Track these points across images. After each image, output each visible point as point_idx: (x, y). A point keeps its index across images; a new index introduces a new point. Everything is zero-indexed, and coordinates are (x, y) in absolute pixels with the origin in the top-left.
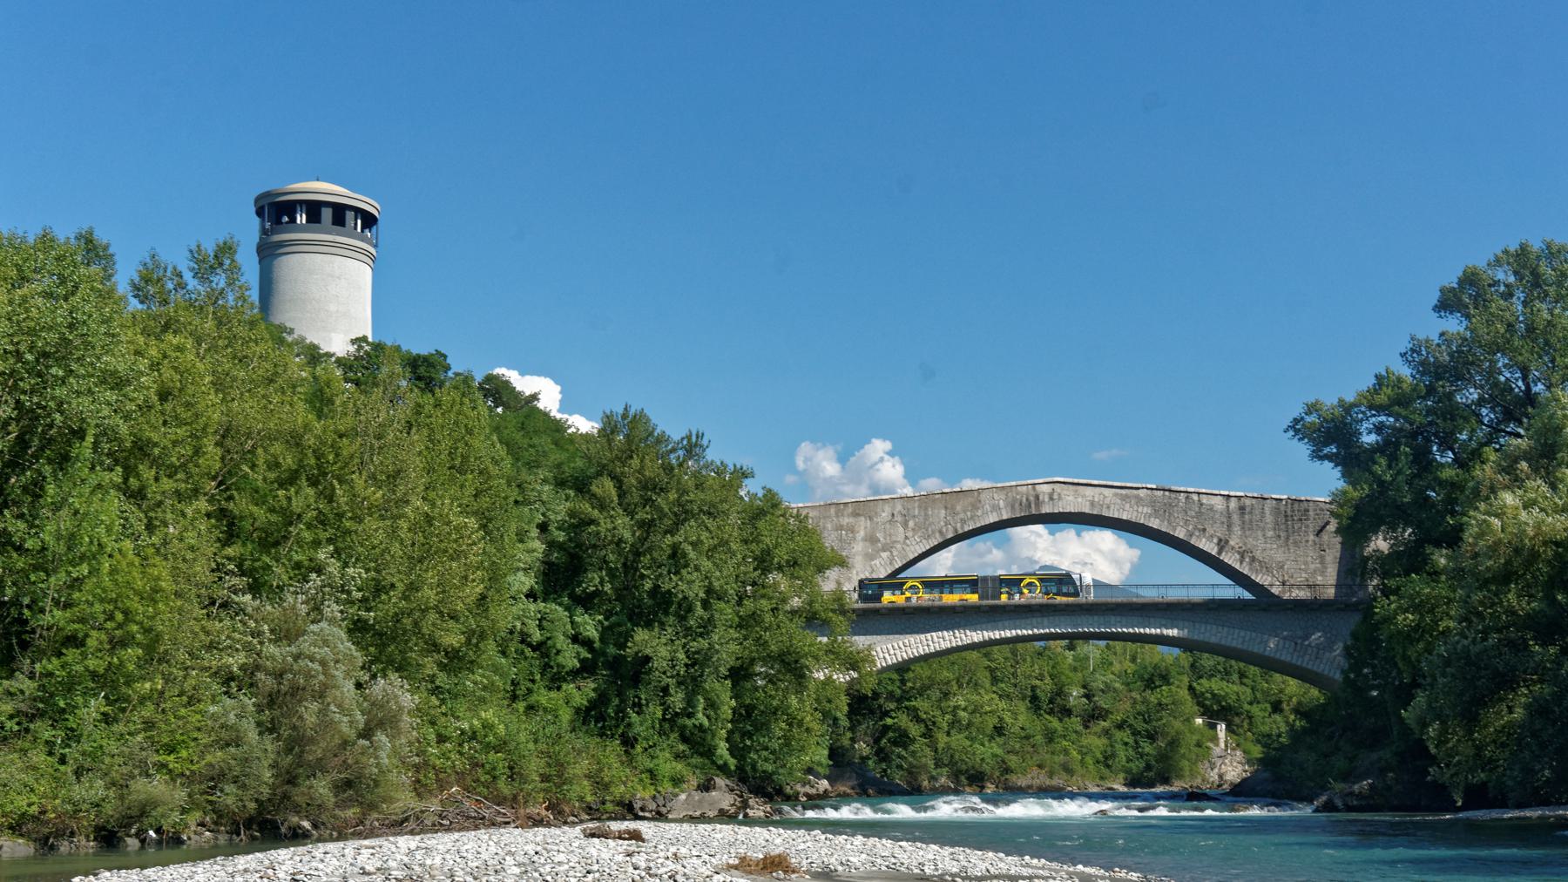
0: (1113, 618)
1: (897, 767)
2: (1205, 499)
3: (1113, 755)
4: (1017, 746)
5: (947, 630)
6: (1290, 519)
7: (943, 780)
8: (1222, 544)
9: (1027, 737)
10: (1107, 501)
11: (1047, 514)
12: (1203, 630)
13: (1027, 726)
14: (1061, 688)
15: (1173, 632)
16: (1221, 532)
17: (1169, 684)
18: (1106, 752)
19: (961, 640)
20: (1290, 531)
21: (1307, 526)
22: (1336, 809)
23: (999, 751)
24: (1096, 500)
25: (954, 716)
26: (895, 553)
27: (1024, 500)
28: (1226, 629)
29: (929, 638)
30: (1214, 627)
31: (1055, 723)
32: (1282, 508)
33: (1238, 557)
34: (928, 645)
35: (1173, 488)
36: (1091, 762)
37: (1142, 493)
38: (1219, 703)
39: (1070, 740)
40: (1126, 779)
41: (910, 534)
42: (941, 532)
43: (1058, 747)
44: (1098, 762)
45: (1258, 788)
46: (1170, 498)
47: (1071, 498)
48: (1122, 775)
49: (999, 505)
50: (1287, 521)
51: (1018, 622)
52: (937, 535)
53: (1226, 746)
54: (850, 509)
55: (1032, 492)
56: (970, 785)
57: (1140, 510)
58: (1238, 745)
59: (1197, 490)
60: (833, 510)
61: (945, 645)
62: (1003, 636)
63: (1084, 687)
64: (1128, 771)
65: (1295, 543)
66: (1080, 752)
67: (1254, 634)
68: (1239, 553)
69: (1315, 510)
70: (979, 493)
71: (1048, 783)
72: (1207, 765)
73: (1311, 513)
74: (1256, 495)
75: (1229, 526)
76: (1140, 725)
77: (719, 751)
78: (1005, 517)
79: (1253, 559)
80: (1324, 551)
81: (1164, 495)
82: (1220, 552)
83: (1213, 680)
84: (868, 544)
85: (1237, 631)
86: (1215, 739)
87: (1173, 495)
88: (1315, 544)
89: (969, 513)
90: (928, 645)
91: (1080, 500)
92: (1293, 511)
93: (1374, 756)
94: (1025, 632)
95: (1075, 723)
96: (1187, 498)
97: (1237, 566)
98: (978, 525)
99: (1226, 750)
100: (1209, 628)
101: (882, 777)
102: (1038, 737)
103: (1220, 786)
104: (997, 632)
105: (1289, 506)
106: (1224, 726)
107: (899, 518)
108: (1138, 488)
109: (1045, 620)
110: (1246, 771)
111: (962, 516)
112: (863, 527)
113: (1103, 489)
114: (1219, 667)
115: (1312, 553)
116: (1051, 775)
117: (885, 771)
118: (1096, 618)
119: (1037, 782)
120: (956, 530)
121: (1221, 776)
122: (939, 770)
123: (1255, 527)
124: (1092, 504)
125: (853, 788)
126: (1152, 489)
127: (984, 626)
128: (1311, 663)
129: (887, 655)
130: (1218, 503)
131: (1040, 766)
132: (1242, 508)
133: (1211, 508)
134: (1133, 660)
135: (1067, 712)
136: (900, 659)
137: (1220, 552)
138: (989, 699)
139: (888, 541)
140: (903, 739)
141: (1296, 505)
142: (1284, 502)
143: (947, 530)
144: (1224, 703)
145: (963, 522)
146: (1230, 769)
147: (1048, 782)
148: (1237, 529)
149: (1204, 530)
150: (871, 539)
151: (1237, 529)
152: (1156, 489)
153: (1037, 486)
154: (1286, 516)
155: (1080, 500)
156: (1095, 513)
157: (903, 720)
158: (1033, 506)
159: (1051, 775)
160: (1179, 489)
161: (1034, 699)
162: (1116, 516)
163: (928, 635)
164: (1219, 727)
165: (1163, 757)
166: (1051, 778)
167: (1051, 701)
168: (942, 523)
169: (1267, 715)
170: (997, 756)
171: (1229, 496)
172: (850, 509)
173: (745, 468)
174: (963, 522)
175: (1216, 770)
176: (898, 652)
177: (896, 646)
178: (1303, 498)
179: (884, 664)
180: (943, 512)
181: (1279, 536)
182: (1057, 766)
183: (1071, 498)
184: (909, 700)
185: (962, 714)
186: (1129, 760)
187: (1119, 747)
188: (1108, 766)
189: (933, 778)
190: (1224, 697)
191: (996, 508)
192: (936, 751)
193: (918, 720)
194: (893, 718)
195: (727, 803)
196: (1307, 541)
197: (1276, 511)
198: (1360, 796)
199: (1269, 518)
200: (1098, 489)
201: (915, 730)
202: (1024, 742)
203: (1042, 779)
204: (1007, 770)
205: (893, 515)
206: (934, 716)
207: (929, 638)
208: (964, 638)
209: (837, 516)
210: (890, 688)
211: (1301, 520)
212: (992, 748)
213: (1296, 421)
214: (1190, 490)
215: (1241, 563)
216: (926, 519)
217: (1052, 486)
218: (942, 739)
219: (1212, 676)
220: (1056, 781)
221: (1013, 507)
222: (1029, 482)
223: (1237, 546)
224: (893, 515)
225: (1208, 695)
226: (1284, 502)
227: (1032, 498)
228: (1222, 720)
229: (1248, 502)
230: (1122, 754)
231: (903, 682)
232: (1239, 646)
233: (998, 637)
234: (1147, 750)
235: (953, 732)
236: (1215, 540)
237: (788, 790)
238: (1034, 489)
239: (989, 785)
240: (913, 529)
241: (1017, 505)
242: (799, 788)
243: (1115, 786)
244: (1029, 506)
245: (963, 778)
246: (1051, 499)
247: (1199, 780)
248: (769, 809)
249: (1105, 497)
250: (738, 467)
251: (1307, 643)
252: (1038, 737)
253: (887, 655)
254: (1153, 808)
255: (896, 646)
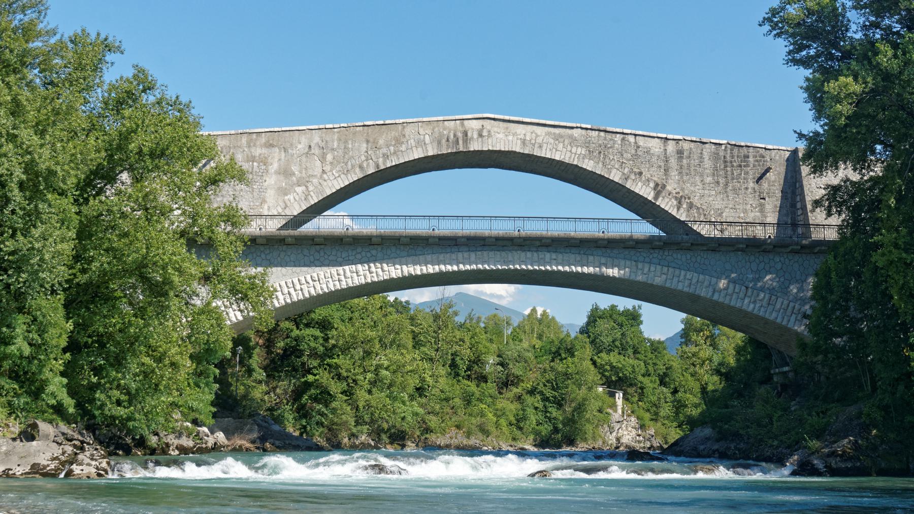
0: (548, 255)
1: (317, 423)
2: (641, 141)
3: (524, 418)
4: (437, 407)
5: (361, 263)
6: (729, 164)
7: (363, 438)
8: (659, 189)
9: (447, 400)
10: (539, 140)
11: (474, 151)
12: (646, 270)
13: (447, 388)
14: (479, 356)
15: (613, 272)
16: (657, 176)
17: (573, 356)
18: (517, 415)
19: (377, 275)
20: (729, 177)
21: (747, 173)
22: (815, 472)
23: (421, 411)
24: (528, 138)
25: (377, 375)
26: (311, 188)
27: (452, 136)
28: (671, 270)
29: (341, 272)
30: (659, 267)
31: (472, 387)
32: (722, 154)
33: (675, 203)
34: (339, 280)
35: (609, 129)
36: (505, 424)
37: (576, 133)
38: (617, 374)
39: (485, 404)
40: (535, 440)
41: (327, 168)
42: (361, 167)
43: (475, 409)
44: (511, 424)
45: (702, 447)
46: (605, 139)
47: (501, 136)
48: (532, 437)
49: (424, 140)
50: (726, 167)
51: (441, 257)
52: (357, 170)
53: (623, 413)
54: (263, 139)
55: (460, 128)
56: (391, 443)
57: (574, 150)
58: (632, 412)
59: (633, 132)
60: (244, 140)
61: (358, 281)
62: (425, 271)
63: (499, 356)
64: (537, 433)
65: (734, 189)
66: (495, 415)
67: (701, 277)
68: (676, 198)
69: (755, 157)
70: (404, 127)
71: (465, 442)
72: (607, 429)
73: (751, 159)
74: (694, 139)
75: (666, 171)
76: (549, 393)
77: (51, 388)
78: (430, 153)
79: (691, 206)
80: (764, 199)
81: (599, 136)
82: (656, 197)
83: (612, 354)
84: (282, 178)
85: (683, 273)
86: (614, 406)
87: (609, 136)
88: (755, 192)
89: (392, 148)
90: (339, 280)
91: (510, 138)
92: (733, 157)
93: (852, 410)
94: (449, 268)
95: (491, 387)
96: (623, 139)
97: (674, 212)
98: (402, 161)
99: (623, 416)
100: (652, 269)
101: (301, 434)
102: (457, 400)
103: (617, 448)
104: (418, 268)
105: (729, 152)
106: (621, 395)
107: (316, 151)
108: (572, 128)
109: (473, 255)
110: (639, 435)
111: (384, 150)
112: (276, 158)
113: (535, 128)
114: (617, 343)
115: (752, 201)
116: (468, 435)
117: (305, 427)
118: (529, 254)
119: (455, 442)
120: (378, 166)
121: (618, 439)
122: (359, 428)
123: (693, 173)
124: (524, 142)
125: (253, 442)
126: (587, 129)
127: (403, 260)
128: (762, 309)
129: (292, 290)
130: (655, 146)
131: (458, 427)
132: (680, 152)
133: (648, 152)
134: (540, 337)
135: (483, 379)
136: (307, 295)
137: (656, 197)
138: (410, 357)
139: (304, 175)
140: (325, 397)
141: (736, 150)
142: (723, 147)
143: (368, 165)
144: (621, 375)
145: (386, 157)
146: (625, 433)
147: (465, 442)
148: (674, 173)
149: (641, 174)
150: (286, 172)
151: (674, 173)
152: (591, 129)
153: (466, 122)
154: (725, 162)
155: (510, 138)
156: (526, 152)
157: (324, 377)
158: (461, 142)
159: (468, 435)
160: (615, 130)
161: (453, 365)
162: (548, 156)
163: (340, 269)
164: (617, 395)
165: (570, 421)
166: (468, 437)
167: (469, 369)
168: (363, 158)
169: (656, 386)
170: (417, 414)
171: (666, 138)
172: (263, 139)
173: (110, 39)
174: (386, 157)
175: (614, 434)
176: (305, 287)
177: (303, 281)
178: (743, 144)
179: (289, 301)
180: (365, 145)
181: (718, 183)
182: (473, 427)
183: (501, 136)
184: (331, 357)
185: (384, 373)
186: (539, 424)
187: (530, 411)
188: (521, 429)
189: (353, 435)
190: (621, 369)
191: (421, 143)
192: (357, 408)
193: (339, 377)
194: (315, 375)
195: (48, 455)
196: (747, 188)
197: (715, 157)
198: (844, 456)
199: (708, 163)
200: (530, 127)
201: (335, 387)
202: (444, 403)
203: (460, 439)
204: (428, 430)
205: (310, 147)
206: (355, 375)
207: (341, 272)
208: (380, 273)
209: (249, 146)
210: (312, 344)
211: (740, 166)
212: (412, 406)
213: (774, 12)
214: (626, 131)
215: (678, 209)
216: (345, 153)
217: (481, 122)
218: (362, 396)
219: (610, 350)
220: (473, 441)
221: (439, 143)
222: (457, 117)
223: (674, 192)
224: (310, 147)
225: (608, 367)
226: (723, 147)
227: (460, 135)
228: (621, 390)
229: (686, 146)
230: (533, 417)
231: (326, 339)
232: (686, 289)
233: (419, 273)
234: (554, 414)
235: (374, 390)
236: (652, 185)
237: (153, 441)
238: (463, 125)
239: (409, 443)
240: (331, 163)
241: (444, 141)
242: (172, 440)
243: (526, 447)
244: (457, 142)
245: (384, 436)
246: (480, 135)
247: (600, 442)
248: (104, 465)
249: (537, 136)
250: (103, 36)
251: (759, 284)
252: (457, 400)
253: (292, 290)
254: (605, 469)
255: (303, 281)
